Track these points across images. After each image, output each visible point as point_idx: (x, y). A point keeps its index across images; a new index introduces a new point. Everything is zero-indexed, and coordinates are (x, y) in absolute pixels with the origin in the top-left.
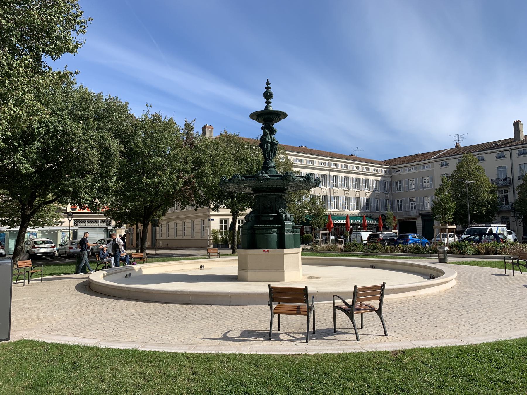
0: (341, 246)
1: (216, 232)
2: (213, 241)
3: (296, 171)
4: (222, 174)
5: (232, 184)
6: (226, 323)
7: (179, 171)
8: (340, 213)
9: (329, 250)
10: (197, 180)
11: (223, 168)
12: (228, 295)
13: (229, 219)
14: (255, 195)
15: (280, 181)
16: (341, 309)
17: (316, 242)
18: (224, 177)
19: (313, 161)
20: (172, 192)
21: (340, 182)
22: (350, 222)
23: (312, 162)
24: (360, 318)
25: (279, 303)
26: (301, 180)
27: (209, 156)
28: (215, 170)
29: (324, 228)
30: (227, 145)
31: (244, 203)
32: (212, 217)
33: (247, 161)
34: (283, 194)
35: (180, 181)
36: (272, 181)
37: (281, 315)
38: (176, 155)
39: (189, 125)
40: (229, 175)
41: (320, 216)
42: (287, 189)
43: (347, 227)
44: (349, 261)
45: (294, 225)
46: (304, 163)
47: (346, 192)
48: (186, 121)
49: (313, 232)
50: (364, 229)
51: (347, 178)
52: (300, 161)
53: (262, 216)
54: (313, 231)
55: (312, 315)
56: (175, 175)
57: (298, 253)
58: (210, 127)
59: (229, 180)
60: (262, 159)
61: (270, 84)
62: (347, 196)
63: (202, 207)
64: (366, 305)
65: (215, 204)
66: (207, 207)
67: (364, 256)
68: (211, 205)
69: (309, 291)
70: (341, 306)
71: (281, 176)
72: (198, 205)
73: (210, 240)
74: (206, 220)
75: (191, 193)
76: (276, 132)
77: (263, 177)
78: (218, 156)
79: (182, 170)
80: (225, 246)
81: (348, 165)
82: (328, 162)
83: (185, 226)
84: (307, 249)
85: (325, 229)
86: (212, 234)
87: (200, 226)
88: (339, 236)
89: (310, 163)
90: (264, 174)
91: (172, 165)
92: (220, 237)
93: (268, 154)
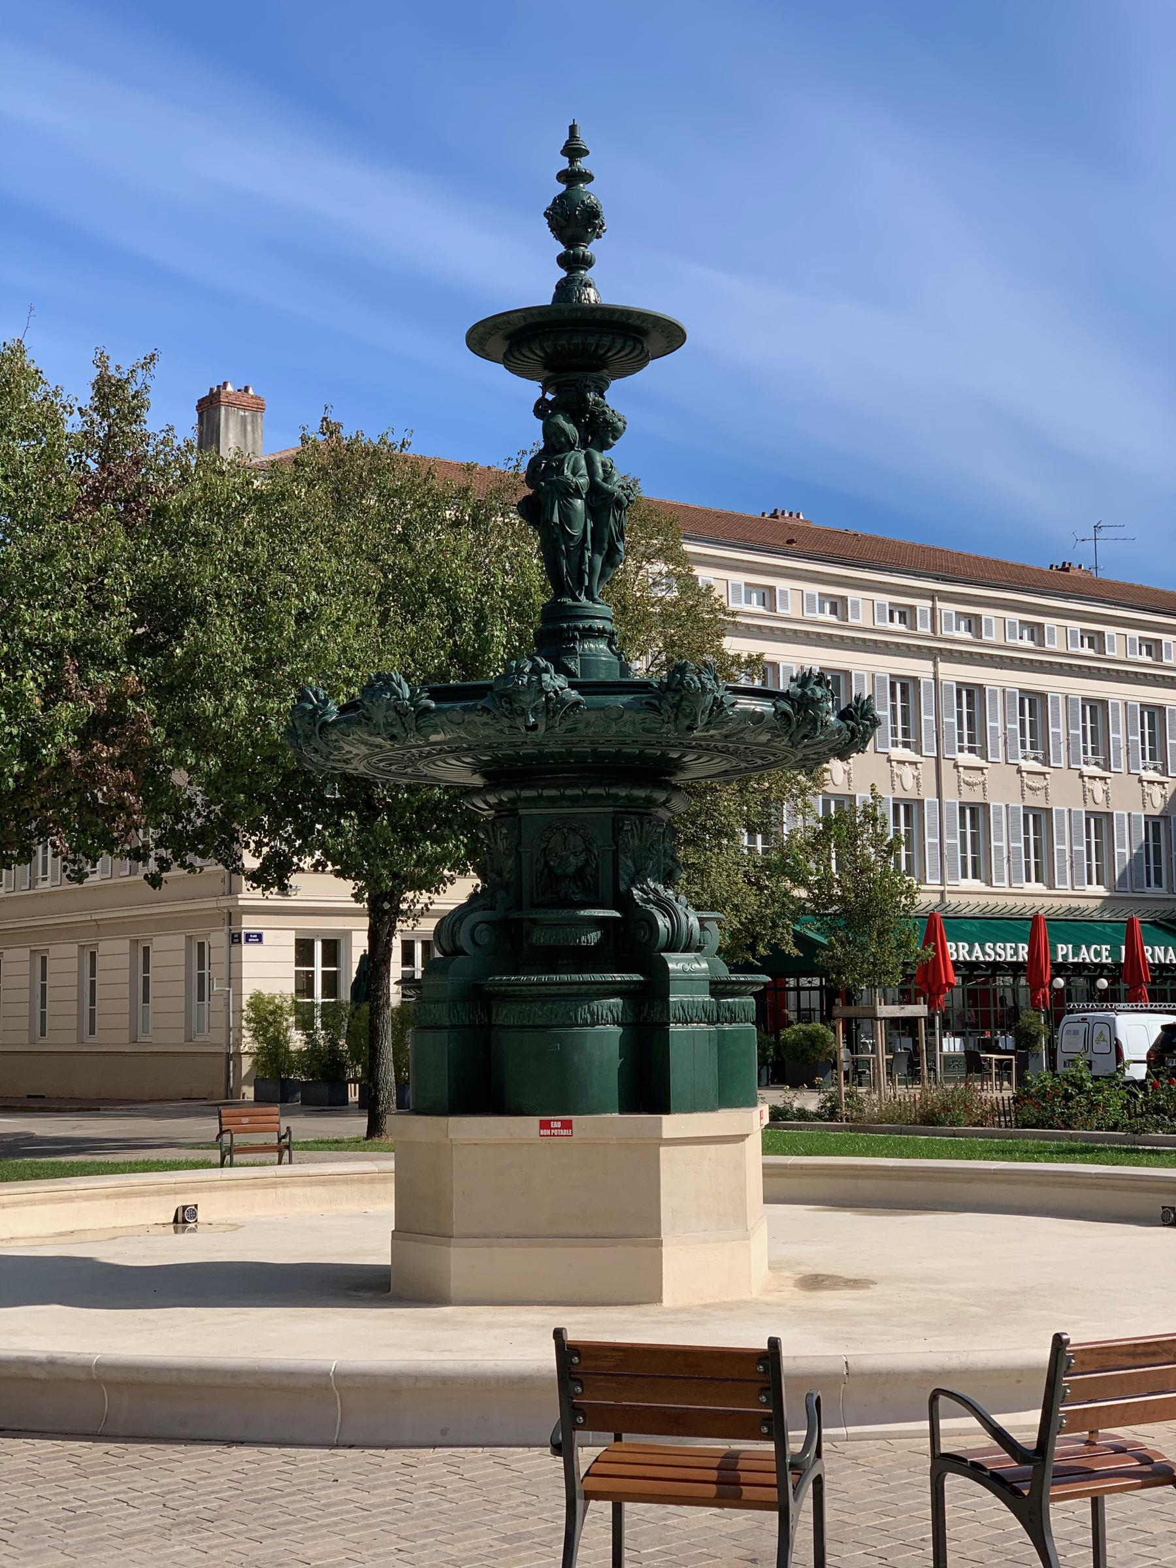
0: (997, 1094)
1: (272, 1013)
2: (255, 1063)
3: (745, 655)
4: (308, 671)
5: (361, 733)
6: (310, 1553)
7: (58, 655)
8: (992, 900)
9: (929, 1119)
10: (159, 707)
11: (315, 638)
12: (327, 1388)
13: (348, 933)
14: (492, 800)
16: (975, 1470)
17: (857, 1074)
18: (316, 694)
19: (844, 599)
20: (16, 778)
21: (995, 720)
22: (1055, 953)
23: (838, 606)
24: (1090, 1523)
25: (618, 1438)
26: (762, 715)
27: (232, 571)
28: (268, 651)
29: (902, 992)
30: (340, 502)
31: (436, 841)
32: (249, 923)
33: (451, 599)
34: (661, 796)
35: (64, 712)
36: (592, 716)
37: (628, 1506)
38: (42, 561)
39: (120, 385)
40: (348, 682)
41: (879, 922)
42: (677, 766)
43: (1036, 984)
44: (1040, 1184)
45: (724, 973)
46: (791, 608)
47: (1029, 780)
48: (102, 363)
49: (836, 1011)
50: (1132, 997)
51: (1035, 701)
52: (768, 596)
53: (534, 922)
54: (839, 1009)
55: (808, 1503)
56: (34, 679)
57: (742, 1138)
58: (245, 400)
59: (343, 710)
60: (543, 588)
61: (586, 153)
62: (1037, 801)
63: (191, 868)
64: (1119, 1450)
65: (265, 850)
66: (221, 867)
67: (1131, 1154)
68: (245, 852)
69: (787, 1365)
70: (977, 1452)
71: (643, 687)
72: (165, 853)
73: (239, 1055)
74: (218, 939)
75: (125, 786)
76: (616, 433)
77: (542, 691)
78: (285, 570)
79: (75, 651)
80: (324, 1091)
81: (1041, 626)
82: (929, 603)
83: (93, 974)
84: (802, 1115)
85: (906, 998)
86: (249, 1021)
87: (181, 973)
88: (988, 1036)
89: (822, 611)
90: (546, 677)
91: (15, 621)
92: (297, 1040)
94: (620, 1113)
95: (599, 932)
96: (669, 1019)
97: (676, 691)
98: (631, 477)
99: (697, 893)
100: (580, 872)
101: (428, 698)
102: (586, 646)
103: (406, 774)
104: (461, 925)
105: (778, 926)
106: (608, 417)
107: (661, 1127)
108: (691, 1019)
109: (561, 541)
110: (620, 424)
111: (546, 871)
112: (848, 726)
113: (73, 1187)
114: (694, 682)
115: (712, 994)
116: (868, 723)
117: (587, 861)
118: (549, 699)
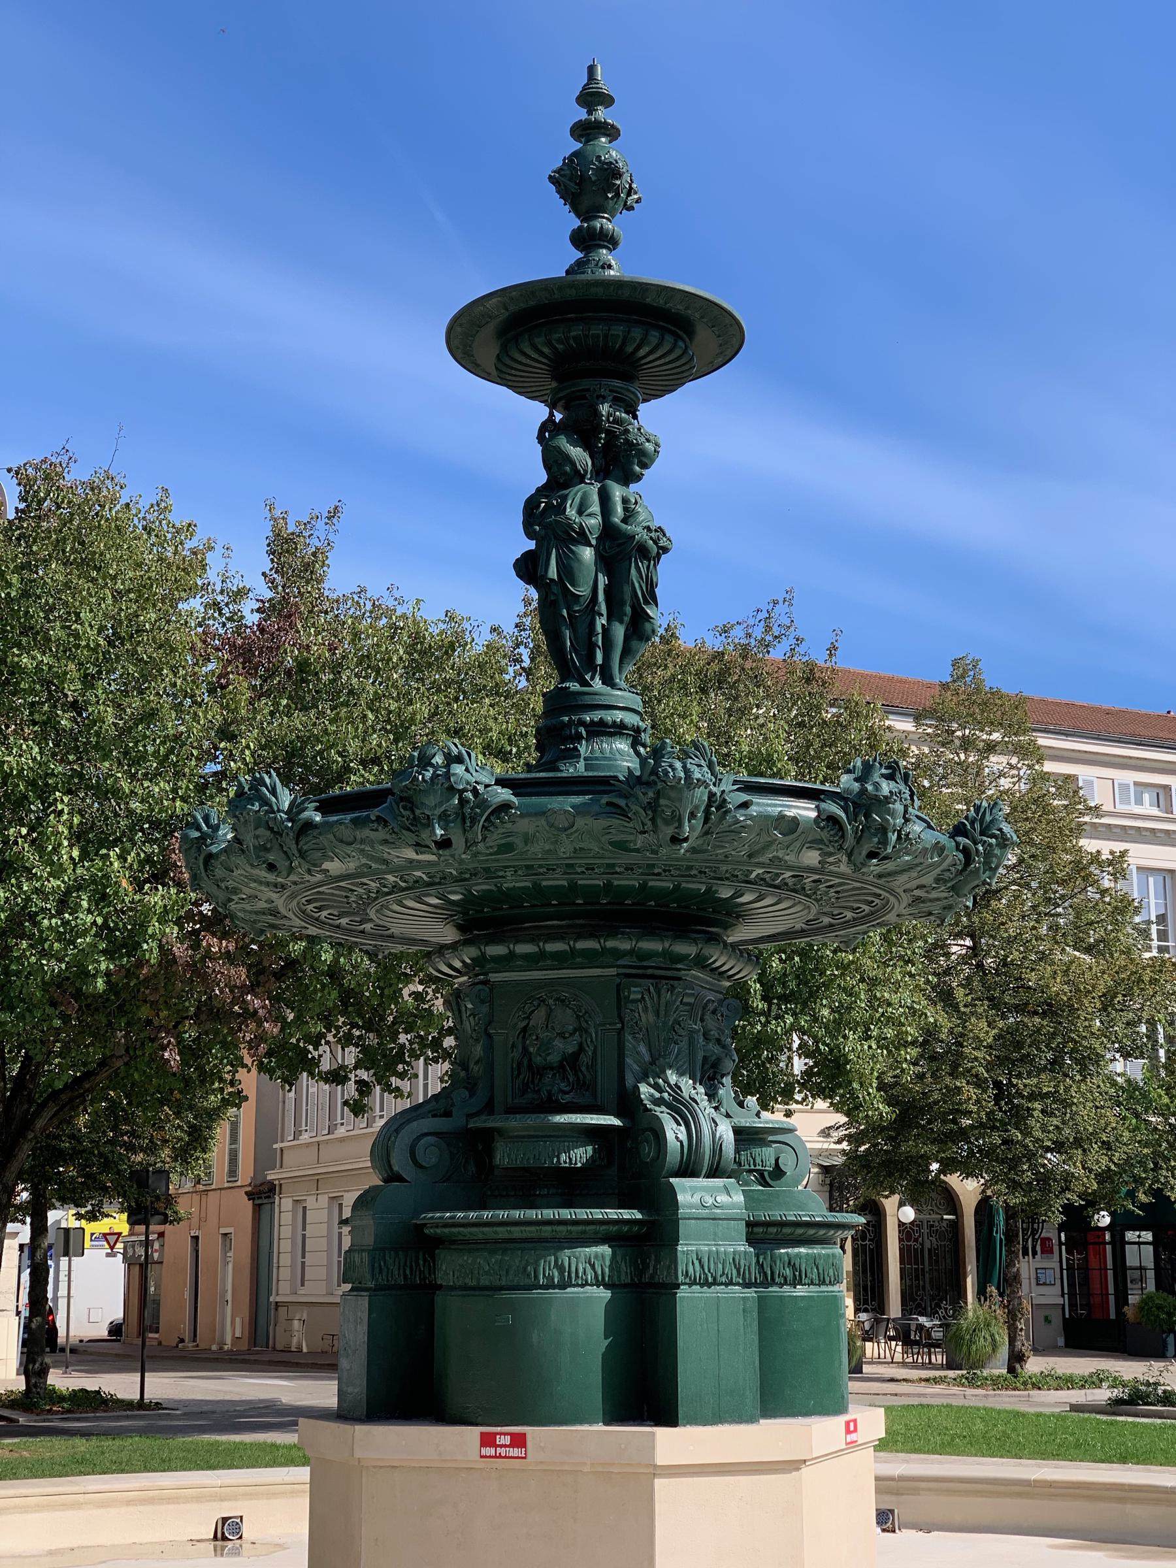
15: (603, 823)
36: (525, 826)
42: (732, 913)
76: (646, 460)
93: (583, 629)
94: (606, 1423)
95: (590, 1149)
96: (677, 1278)
97: (649, 784)
98: (970, 658)
99: (1057, 1127)
100: (572, 1060)
101: (317, 809)
102: (596, 747)
103: (363, 932)
104: (396, 1138)
105: (1161, 1168)
106: (631, 437)
107: (653, 1448)
108: (715, 1279)
109: (562, 603)
110: (649, 447)
111: (525, 1061)
112: (958, 844)
113: (24, 1491)
114: (674, 769)
115: (751, 1240)
116: (993, 841)
117: (581, 1045)
118: (463, 802)
